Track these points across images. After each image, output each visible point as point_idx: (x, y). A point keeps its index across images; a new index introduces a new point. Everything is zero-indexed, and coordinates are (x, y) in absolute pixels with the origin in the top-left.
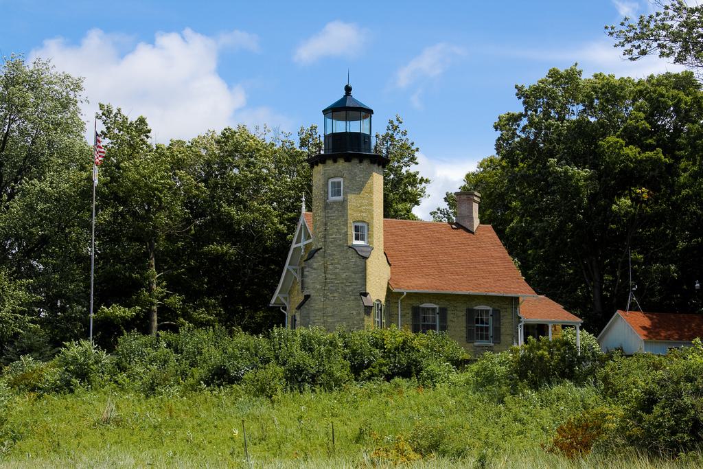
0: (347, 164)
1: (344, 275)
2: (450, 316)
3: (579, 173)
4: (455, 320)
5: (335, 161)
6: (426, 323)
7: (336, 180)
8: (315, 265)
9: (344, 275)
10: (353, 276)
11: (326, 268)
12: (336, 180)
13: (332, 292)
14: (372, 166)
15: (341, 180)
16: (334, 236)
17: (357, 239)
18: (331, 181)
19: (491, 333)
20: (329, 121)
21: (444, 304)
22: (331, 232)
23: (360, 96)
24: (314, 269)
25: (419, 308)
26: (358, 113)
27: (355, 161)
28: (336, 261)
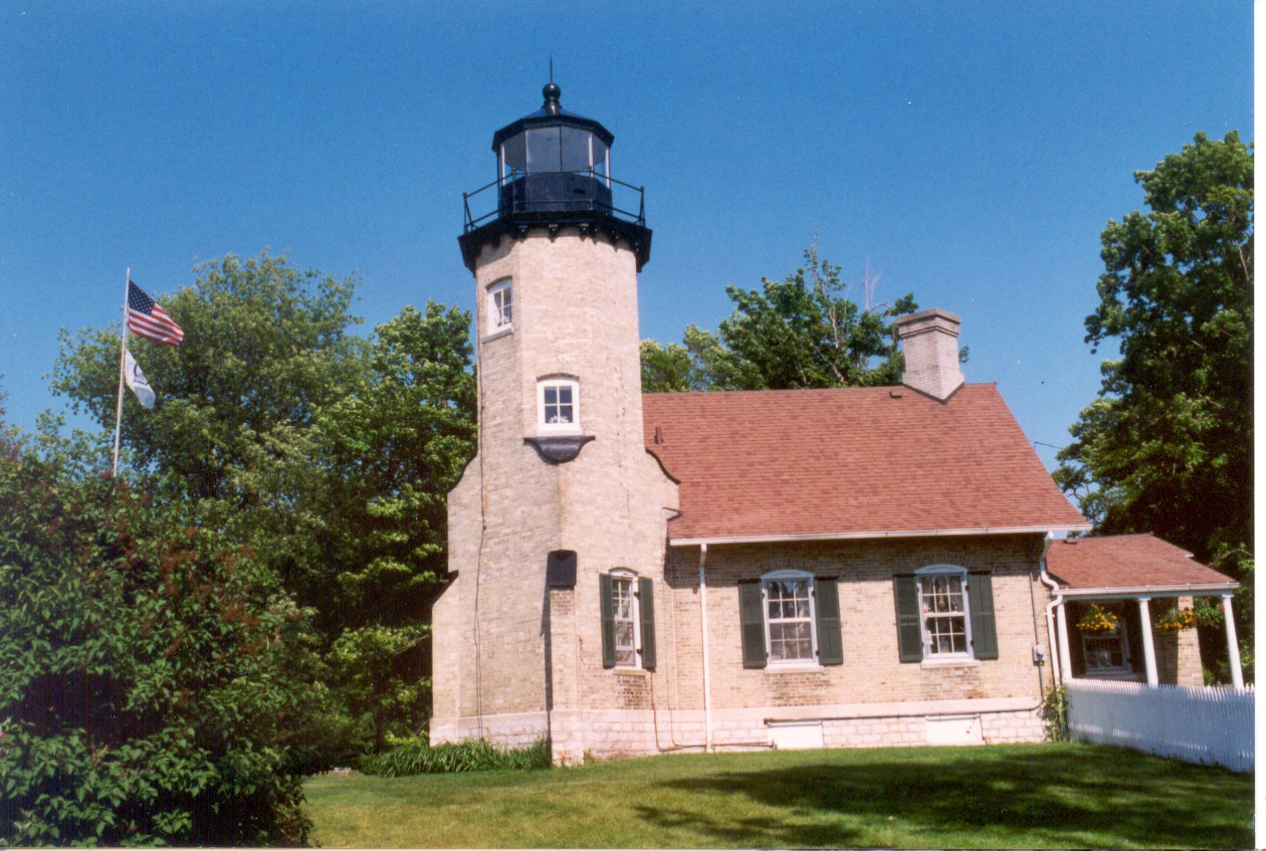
6: (782, 620)
8: (465, 500)
13: (498, 559)
16: (498, 420)
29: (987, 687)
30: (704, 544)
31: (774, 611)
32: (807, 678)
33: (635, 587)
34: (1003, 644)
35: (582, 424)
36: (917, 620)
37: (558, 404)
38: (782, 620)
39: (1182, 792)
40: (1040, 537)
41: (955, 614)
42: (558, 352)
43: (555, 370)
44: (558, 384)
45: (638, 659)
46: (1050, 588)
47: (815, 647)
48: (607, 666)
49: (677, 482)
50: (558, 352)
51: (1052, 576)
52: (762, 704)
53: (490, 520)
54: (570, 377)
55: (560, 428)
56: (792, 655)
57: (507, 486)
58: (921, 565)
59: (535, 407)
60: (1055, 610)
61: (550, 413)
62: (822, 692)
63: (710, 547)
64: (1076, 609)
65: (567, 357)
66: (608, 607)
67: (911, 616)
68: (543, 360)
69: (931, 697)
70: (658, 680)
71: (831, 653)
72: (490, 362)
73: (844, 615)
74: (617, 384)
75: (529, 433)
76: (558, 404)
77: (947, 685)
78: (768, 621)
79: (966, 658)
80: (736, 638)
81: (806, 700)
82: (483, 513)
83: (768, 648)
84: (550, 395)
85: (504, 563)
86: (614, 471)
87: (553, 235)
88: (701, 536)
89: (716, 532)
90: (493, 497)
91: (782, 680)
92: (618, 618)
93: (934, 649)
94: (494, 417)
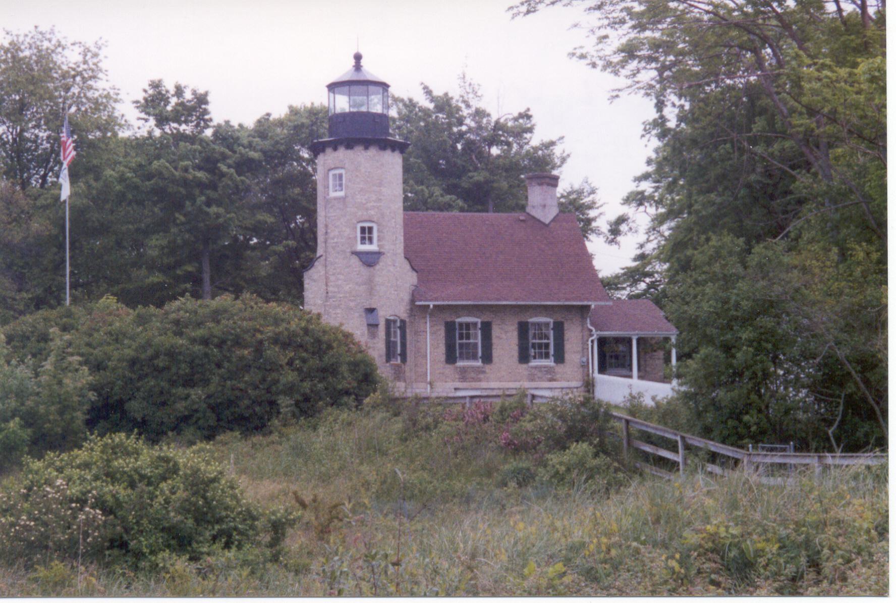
0: (349, 152)
1: (347, 287)
2: (496, 331)
3: (243, 182)
4: (504, 336)
5: (335, 149)
6: (464, 341)
7: (337, 172)
8: (315, 277)
9: (347, 287)
10: (357, 288)
11: (327, 278)
12: (337, 172)
13: (335, 307)
14: (382, 153)
15: (342, 171)
16: (336, 240)
17: (363, 243)
18: (331, 173)
19: (552, 351)
20: (332, 95)
21: (487, 318)
22: (332, 235)
23: (372, 70)
24: (315, 281)
25: (527, 323)
26: (365, 88)
27: (359, 149)
28: (338, 270)
29: (558, 376)
30: (431, 304)
31: (461, 338)
32: (549, 370)
33: (398, 324)
34: (567, 356)
35: (378, 246)
36: (528, 343)
37: (367, 235)
38: (464, 341)
39: (696, 4)
40: (588, 307)
41: (546, 341)
42: (367, 209)
43: (366, 218)
44: (366, 225)
45: (399, 358)
46: (591, 331)
47: (480, 354)
48: (388, 360)
49: (417, 272)
50: (367, 209)
51: (592, 324)
52: (453, 381)
53: (330, 289)
54: (373, 222)
55: (367, 247)
56: (468, 358)
57: (340, 273)
58: (531, 317)
59: (356, 237)
60: (592, 341)
61: (363, 239)
62: (482, 376)
63: (435, 306)
64: (602, 342)
65: (372, 212)
66: (388, 334)
67: (457, 326)
68: (360, 213)
69: (533, 380)
70: (408, 368)
71: (487, 358)
72: (331, 211)
73: (495, 341)
74: (393, 224)
75: (353, 249)
76: (367, 235)
77: (539, 374)
78: (458, 341)
79: (550, 362)
80: (442, 349)
81: (474, 380)
82: (327, 285)
83: (458, 355)
84: (363, 230)
85: (339, 311)
86: (392, 269)
87: (366, 148)
88: (431, 300)
89: (436, 299)
90: (332, 278)
91: (463, 371)
92: (392, 339)
93: (535, 358)
94: (333, 239)
